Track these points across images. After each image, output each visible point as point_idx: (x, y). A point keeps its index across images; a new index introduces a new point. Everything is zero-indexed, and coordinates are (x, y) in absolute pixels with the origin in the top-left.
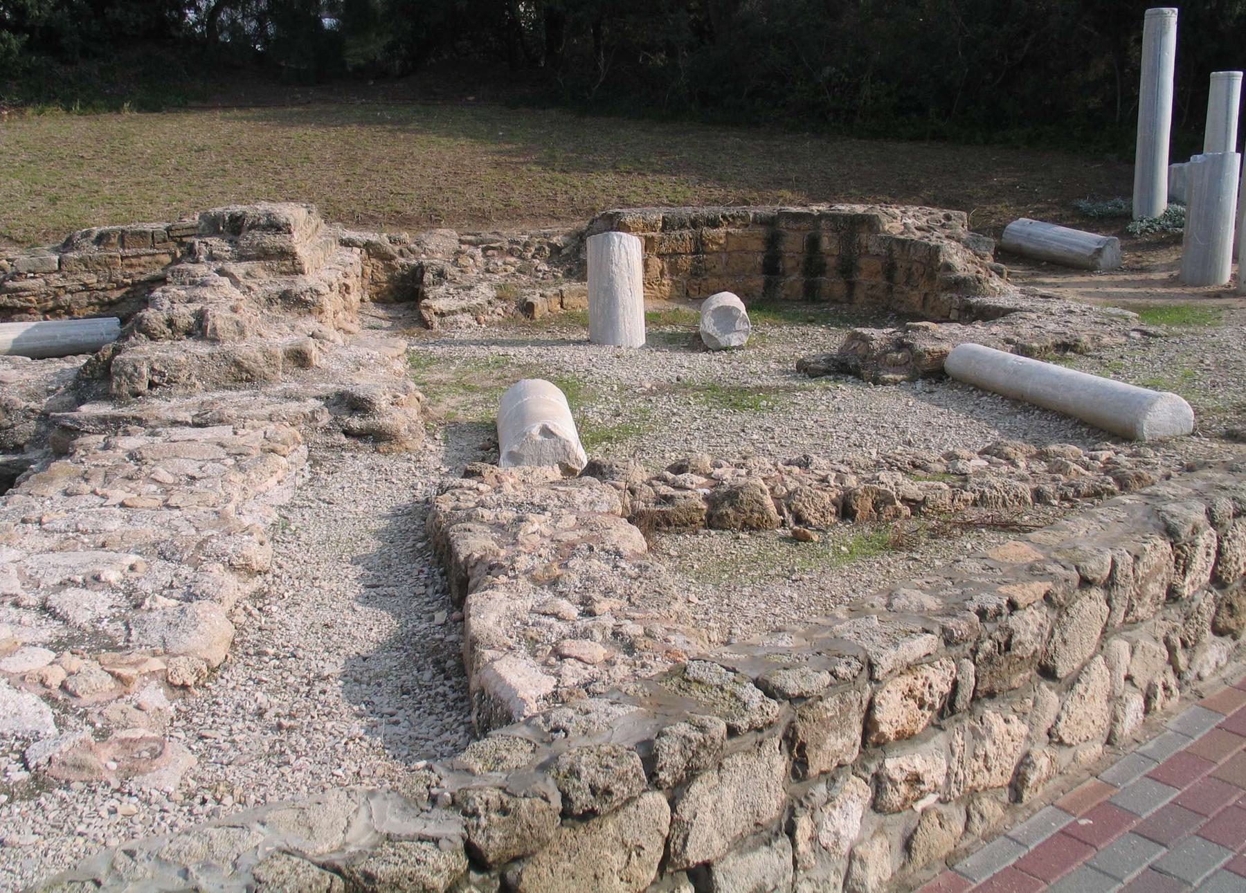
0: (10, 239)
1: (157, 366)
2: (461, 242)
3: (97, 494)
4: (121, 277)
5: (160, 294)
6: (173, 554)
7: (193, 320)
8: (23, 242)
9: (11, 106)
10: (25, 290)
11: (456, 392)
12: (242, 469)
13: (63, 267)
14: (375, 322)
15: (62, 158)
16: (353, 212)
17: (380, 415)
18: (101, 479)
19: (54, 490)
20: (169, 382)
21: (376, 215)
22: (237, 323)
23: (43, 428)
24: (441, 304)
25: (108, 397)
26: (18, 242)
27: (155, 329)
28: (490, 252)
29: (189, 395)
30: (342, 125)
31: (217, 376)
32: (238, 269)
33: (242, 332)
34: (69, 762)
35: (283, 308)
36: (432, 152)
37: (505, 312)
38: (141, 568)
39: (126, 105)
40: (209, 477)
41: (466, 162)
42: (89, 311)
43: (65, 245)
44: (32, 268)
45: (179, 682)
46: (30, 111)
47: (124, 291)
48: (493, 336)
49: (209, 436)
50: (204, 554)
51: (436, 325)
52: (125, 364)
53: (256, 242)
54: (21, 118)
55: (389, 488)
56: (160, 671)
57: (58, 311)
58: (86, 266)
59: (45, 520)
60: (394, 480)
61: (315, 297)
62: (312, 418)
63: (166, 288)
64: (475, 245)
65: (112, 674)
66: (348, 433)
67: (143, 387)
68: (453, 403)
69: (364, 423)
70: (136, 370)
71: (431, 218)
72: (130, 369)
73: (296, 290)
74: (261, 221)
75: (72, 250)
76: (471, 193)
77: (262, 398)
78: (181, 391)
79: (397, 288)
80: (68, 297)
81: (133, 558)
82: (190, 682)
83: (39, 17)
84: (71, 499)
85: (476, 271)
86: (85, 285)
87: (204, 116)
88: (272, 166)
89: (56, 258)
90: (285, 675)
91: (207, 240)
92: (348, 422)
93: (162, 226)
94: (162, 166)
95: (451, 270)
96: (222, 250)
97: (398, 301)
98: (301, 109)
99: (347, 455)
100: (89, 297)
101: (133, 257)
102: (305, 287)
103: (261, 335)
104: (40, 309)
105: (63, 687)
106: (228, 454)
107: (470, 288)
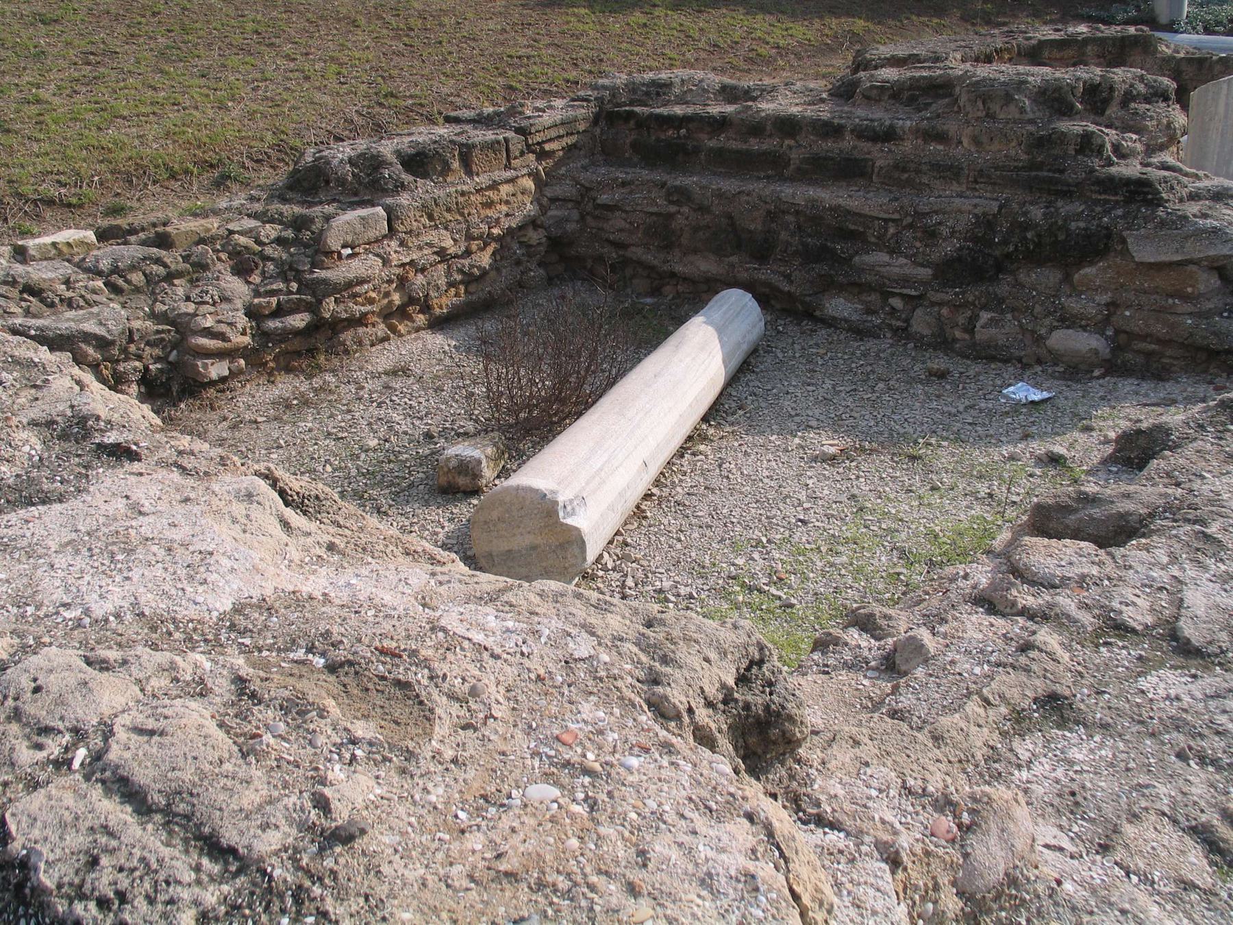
44: (349, 239)
58: (431, 217)
100: (448, 273)
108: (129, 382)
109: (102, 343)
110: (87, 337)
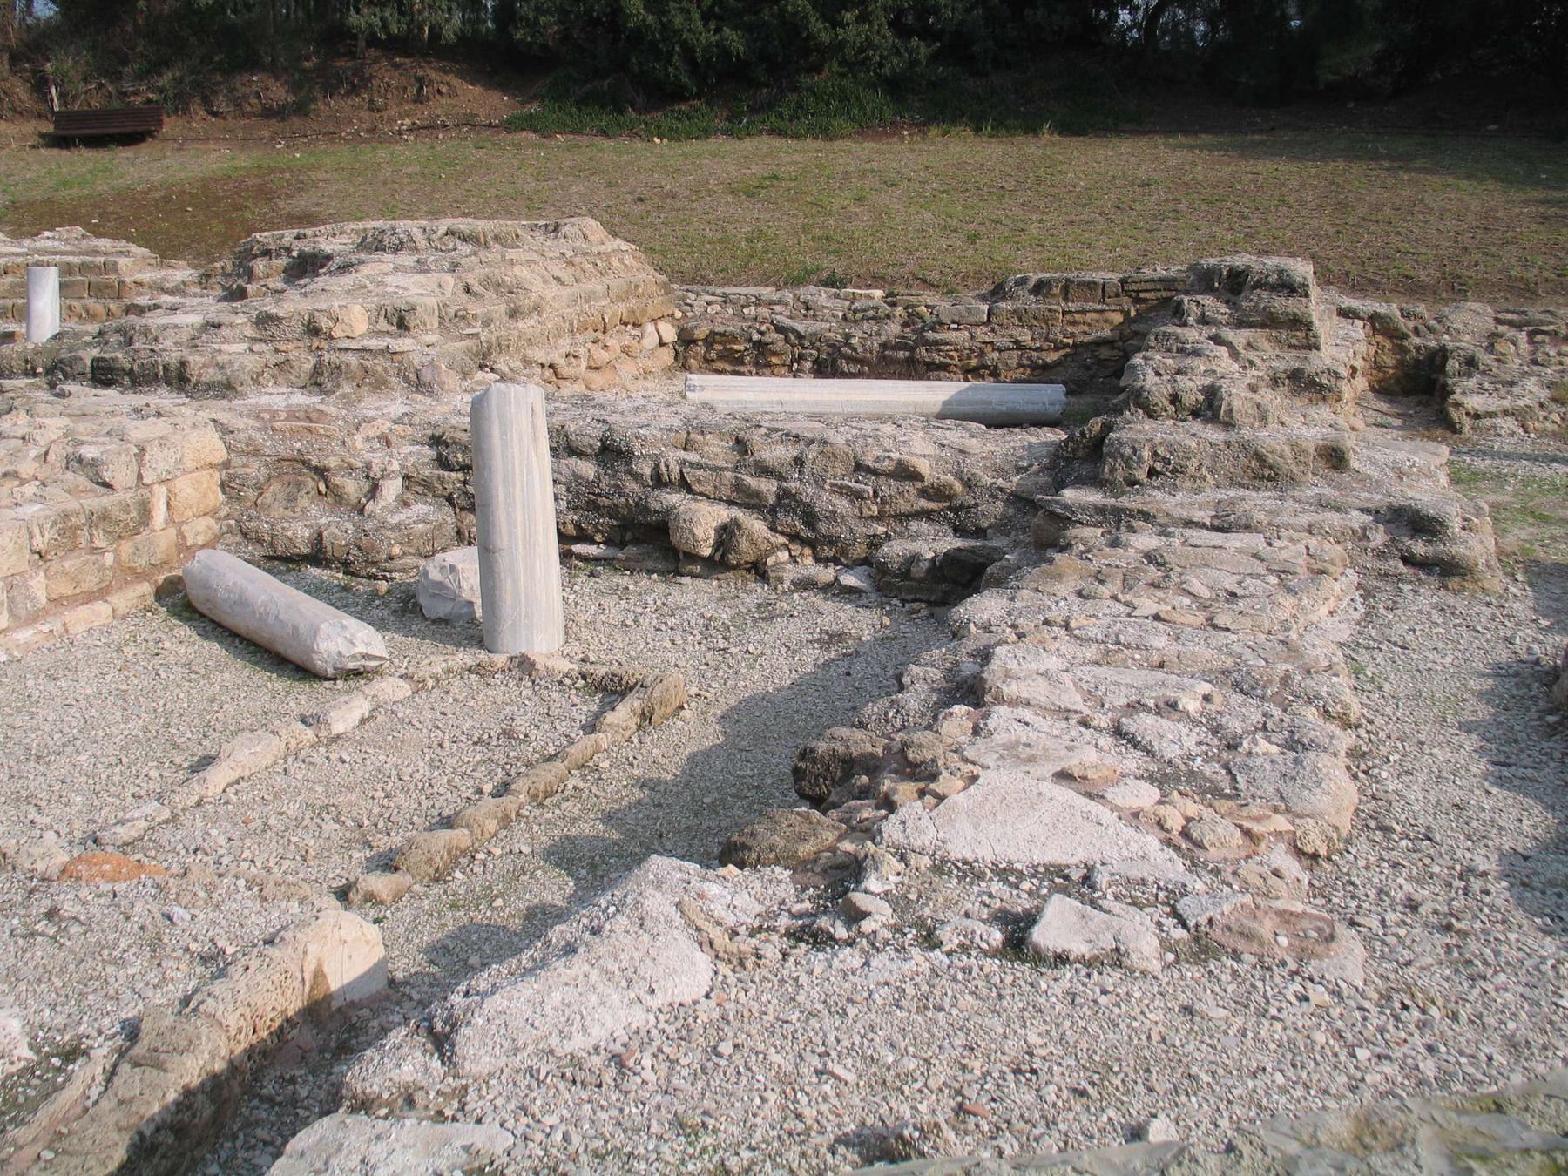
0: (924, 281)
1: (1161, 451)
2: (1498, 321)
3: (1118, 601)
4: (1060, 336)
5: (1142, 362)
6: (1253, 688)
7: (1201, 398)
8: (938, 286)
9: (913, 125)
10: (947, 344)
11: (1524, 520)
12: (1290, 590)
13: (993, 319)
14: (1380, 419)
15: (979, 189)
16: (1347, 274)
17: (1453, 541)
18: (1119, 582)
19: (1066, 588)
20: (1174, 471)
21: (1378, 278)
22: (1258, 406)
23: (1011, 512)
24: (1475, 402)
25: (1096, 482)
26: (933, 285)
27: (1157, 404)
28: (1539, 338)
29: (1198, 491)
30: (1322, 159)
31: (1232, 470)
32: (1238, 337)
33: (1263, 418)
34: (1235, 927)
35: (1291, 391)
36: (1450, 200)
37: (1562, 419)
38: (1218, 699)
39: (1046, 126)
40: (1252, 596)
41: (1500, 214)
42: (1019, 374)
43: (993, 293)
44: (957, 318)
45: (1309, 849)
46: (934, 131)
47: (1062, 352)
48: (1550, 451)
49: (1239, 545)
50: (1291, 694)
51: (1466, 429)
52: (1121, 444)
53: (1262, 306)
54: (923, 139)
55: (1476, 638)
56: (1288, 832)
57: (981, 372)
58: (1020, 320)
59: (1073, 624)
60: (1479, 628)
61: (1333, 380)
62: (1363, 536)
63: (1149, 354)
64: (1518, 326)
65: (1240, 827)
66: (1408, 560)
67: (1141, 475)
68: (1523, 535)
69: (1430, 549)
70: (1135, 452)
71: (1453, 286)
72: (1128, 451)
73: (1310, 369)
74: (1270, 279)
75: (1003, 299)
76: (1510, 256)
77: (1290, 503)
78: (1188, 484)
79: (1407, 376)
80: (996, 355)
81: (1206, 688)
82: (1323, 852)
83: (952, 19)
84: (1090, 602)
85: (1518, 361)
86: (1016, 342)
87: (1141, 143)
88: (1238, 208)
89: (986, 307)
90: (1427, 861)
91: (1199, 298)
92: (1409, 546)
93: (1115, 277)
94: (1099, 203)
95: (1486, 359)
96: (1218, 312)
97: (1407, 393)
98: (1264, 137)
99: (1406, 588)
100: (1020, 357)
101: (1077, 312)
102: (1321, 367)
103: (1282, 424)
104: (961, 368)
105: (1185, 834)
106: (1268, 569)
107: (1512, 383)
108: (806, 360)
109: (800, 336)
110: (794, 331)
